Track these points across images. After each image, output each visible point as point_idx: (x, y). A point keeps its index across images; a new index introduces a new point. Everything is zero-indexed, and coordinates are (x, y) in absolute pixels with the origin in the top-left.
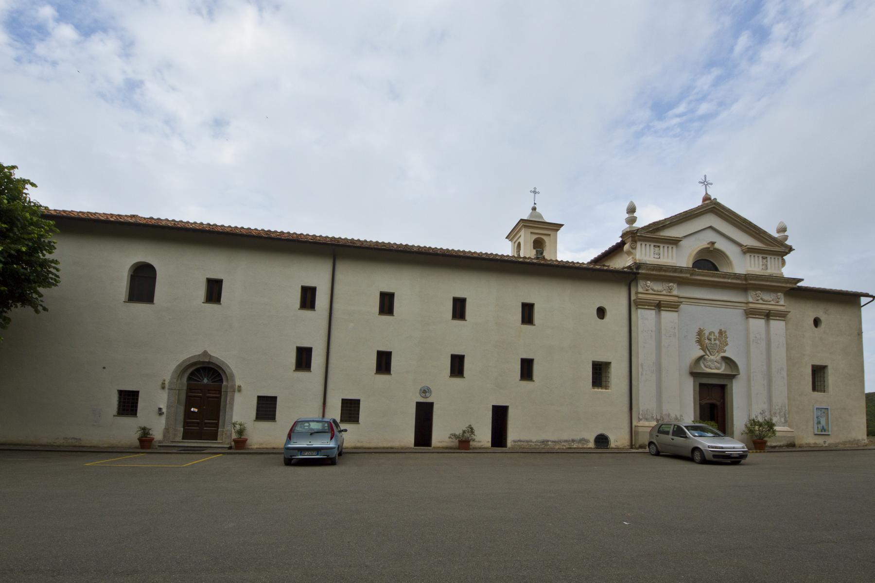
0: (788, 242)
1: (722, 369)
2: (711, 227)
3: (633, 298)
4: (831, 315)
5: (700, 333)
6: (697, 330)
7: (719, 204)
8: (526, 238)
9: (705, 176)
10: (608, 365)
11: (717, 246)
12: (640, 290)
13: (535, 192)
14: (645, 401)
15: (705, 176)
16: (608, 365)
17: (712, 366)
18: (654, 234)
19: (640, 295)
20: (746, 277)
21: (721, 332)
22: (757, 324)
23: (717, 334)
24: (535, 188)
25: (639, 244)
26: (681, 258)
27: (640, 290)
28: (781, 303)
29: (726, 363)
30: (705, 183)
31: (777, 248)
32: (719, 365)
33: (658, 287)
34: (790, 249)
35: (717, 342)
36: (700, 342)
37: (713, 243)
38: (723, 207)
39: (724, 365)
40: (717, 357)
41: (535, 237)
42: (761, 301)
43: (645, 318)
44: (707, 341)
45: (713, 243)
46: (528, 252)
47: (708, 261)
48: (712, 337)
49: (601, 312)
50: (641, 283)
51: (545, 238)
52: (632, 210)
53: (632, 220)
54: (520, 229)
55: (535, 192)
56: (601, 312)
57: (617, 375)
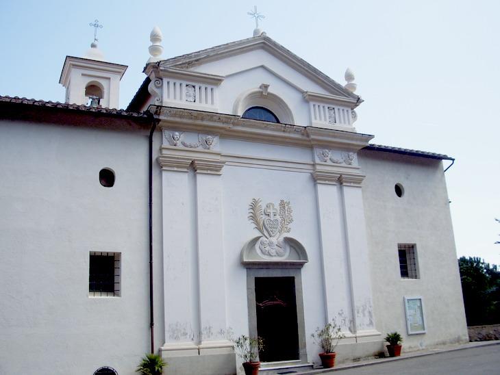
0: (356, 93)
1: (286, 256)
2: (263, 67)
3: (154, 157)
4: (410, 177)
5: (254, 206)
6: (250, 201)
7: (268, 39)
8: (79, 83)
9: (255, 7)
10: (413, 247)
11: (270, 90)
12: (166, 144)
13: (96, 26)
14: (176, 308)
15: (255, 7)
16: (413, 247)
17: (273, 252)
18: (186, 69)
19: (164, 152)
20: (305, 130)
21: (282, 204)
22: (328, 193)
23: (277, 206)
24: (96, 21)
25: (165, 81)
26: (227, 100)
27: (166, 144)
28: (356, 165)
29: (291, 246)
30: (255, 15)
31: (346, 99)
32: (281, 250)
33: (192, 140)
34: (359, 100)
35: (278, 217)
36: (254, 218)
37: (266, 87)
38: (275, 44)
39: (288, 249)
40: (277, 239)
41: (88, 81)
42: (329, 163)
43: (174, 185)
44: (264, 217)
45: (266, 87)
46: (80, 99)
47: (263, 111)
48: (271, 211)
49: (107, 178)
50: (166, 133)
51: (104, 83)
52: (155, 37)
53: (154, 50)
54: (69, 71)
55: (96, 26)
56: (107, 178)
57: (130, 274)
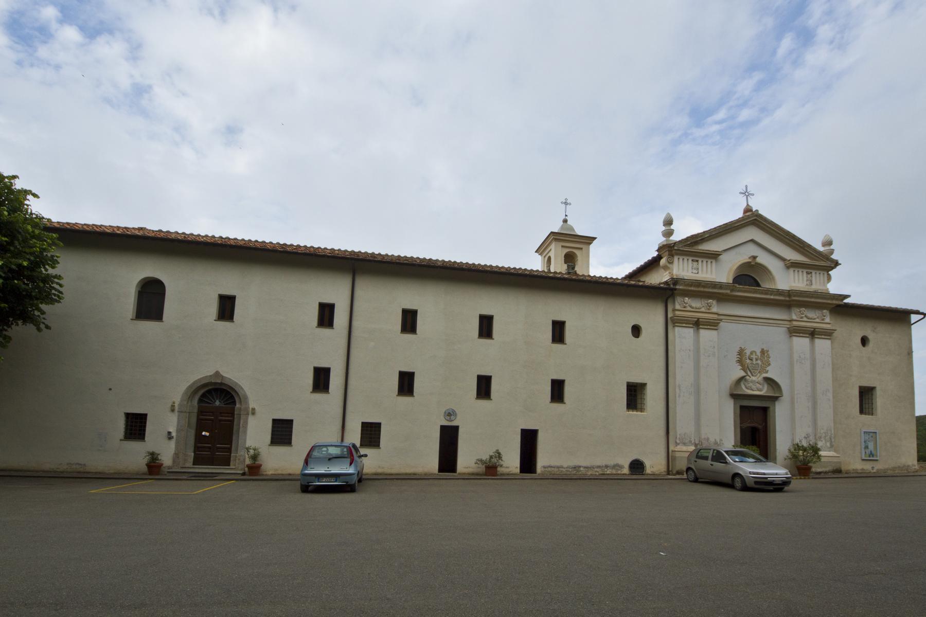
0: (834, 257)
1: (764, 391)
2: (752, 241)
3: (670, 315)
4: (880, 334)
5: (741, 352)
6: (738, 349)
7: (760, 216)
8: (557, 252)
9: (746, 187)
10: (643, 386)
11: (758, 260)
12: (678, 307)
13: (566, 203)
15: (746, 187)
16: (643, 386)
17: (754, 387)
19: (677, 313)
20: (790, 293)
21: (763, 352)
22: (801, 343)
23: (759, 354)
24: (566, 199)
25: (676, 258)
26: (721, 273)
27: (678, 307)
28: (826, 320)
29: (768, 384)
30: (746, 194)
31: (822, 262)
32: (761, 387)
33: (696, 303)
34: (836, 264)
35: (759, 362)
36: (740, 362)
37: (755, 258)
38: (765, 219)
39: (766, 386)
40: (758, 378)
41: (566, 251)
42: (805, 319)
43: (683, 336)
44: (748, 361)
45: (755, 258)
46: (559, 267)
47: (749, 276)
48: (754, 357)
49: (636, 331)
50: (679, 300)
51: (577, 252)
52: (668, 222)
53: (668, 233)
54: (551, 243)
55: (566, 203)
56: (636, 331)
57: (653, 397)
